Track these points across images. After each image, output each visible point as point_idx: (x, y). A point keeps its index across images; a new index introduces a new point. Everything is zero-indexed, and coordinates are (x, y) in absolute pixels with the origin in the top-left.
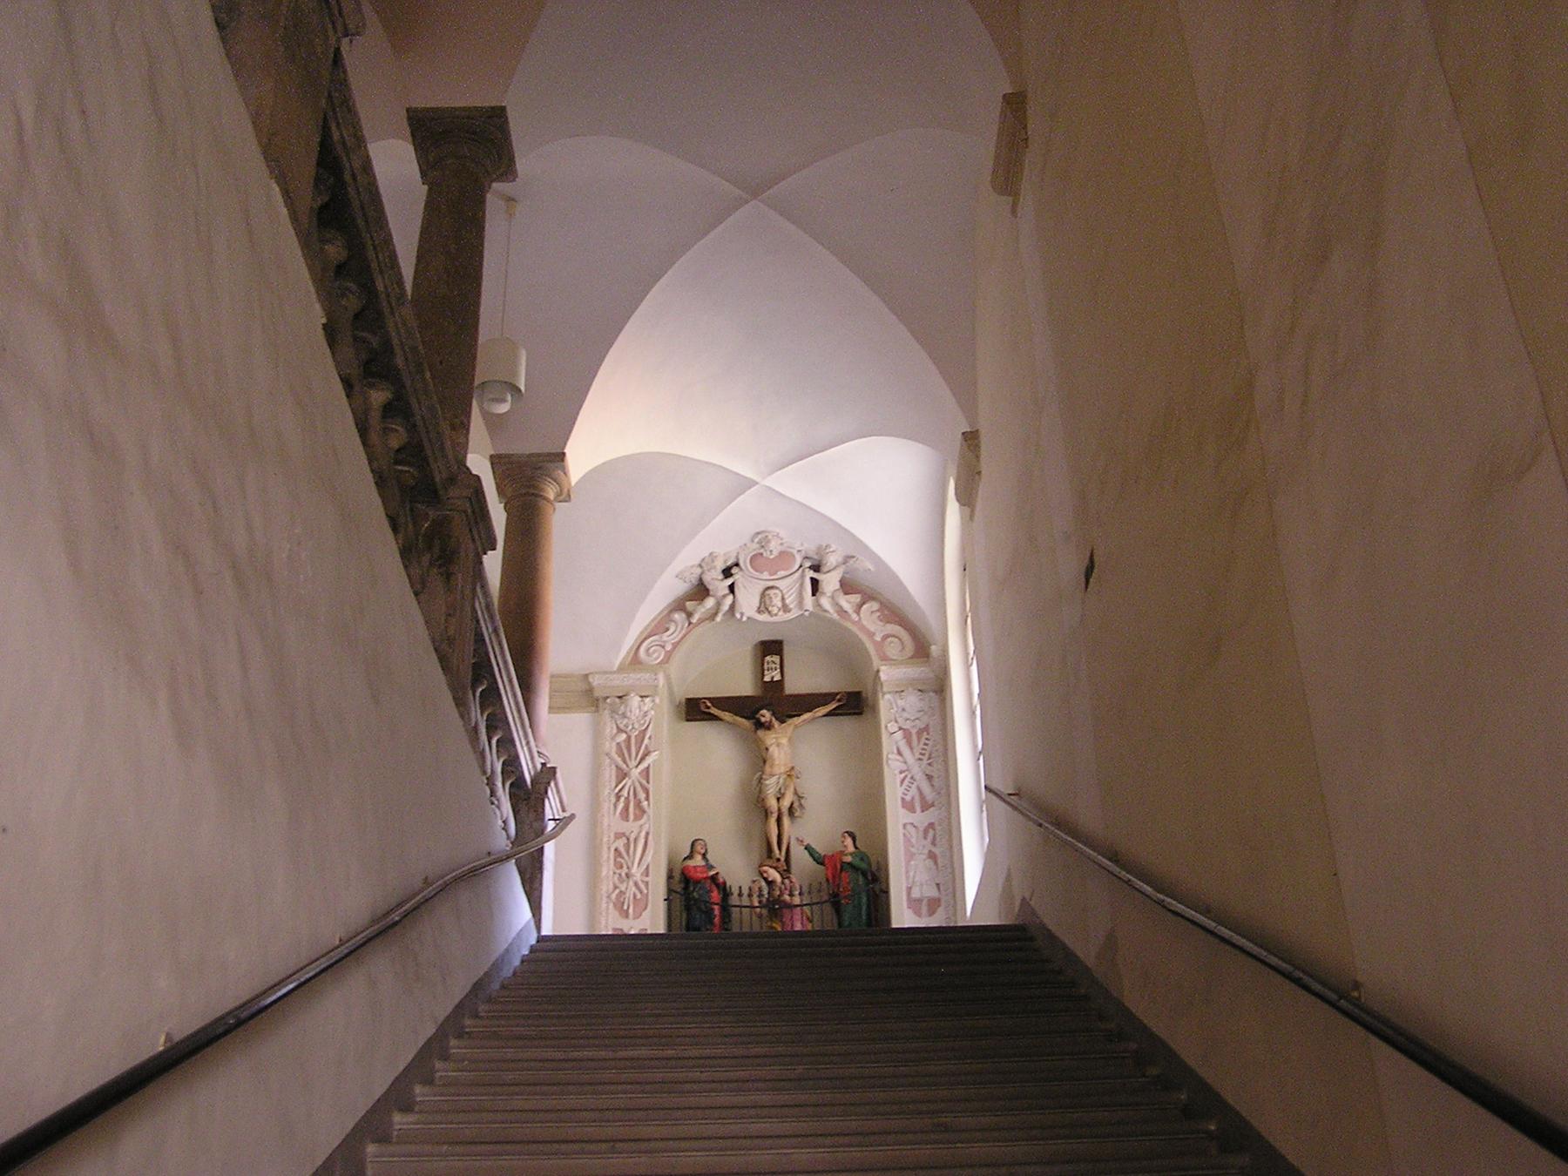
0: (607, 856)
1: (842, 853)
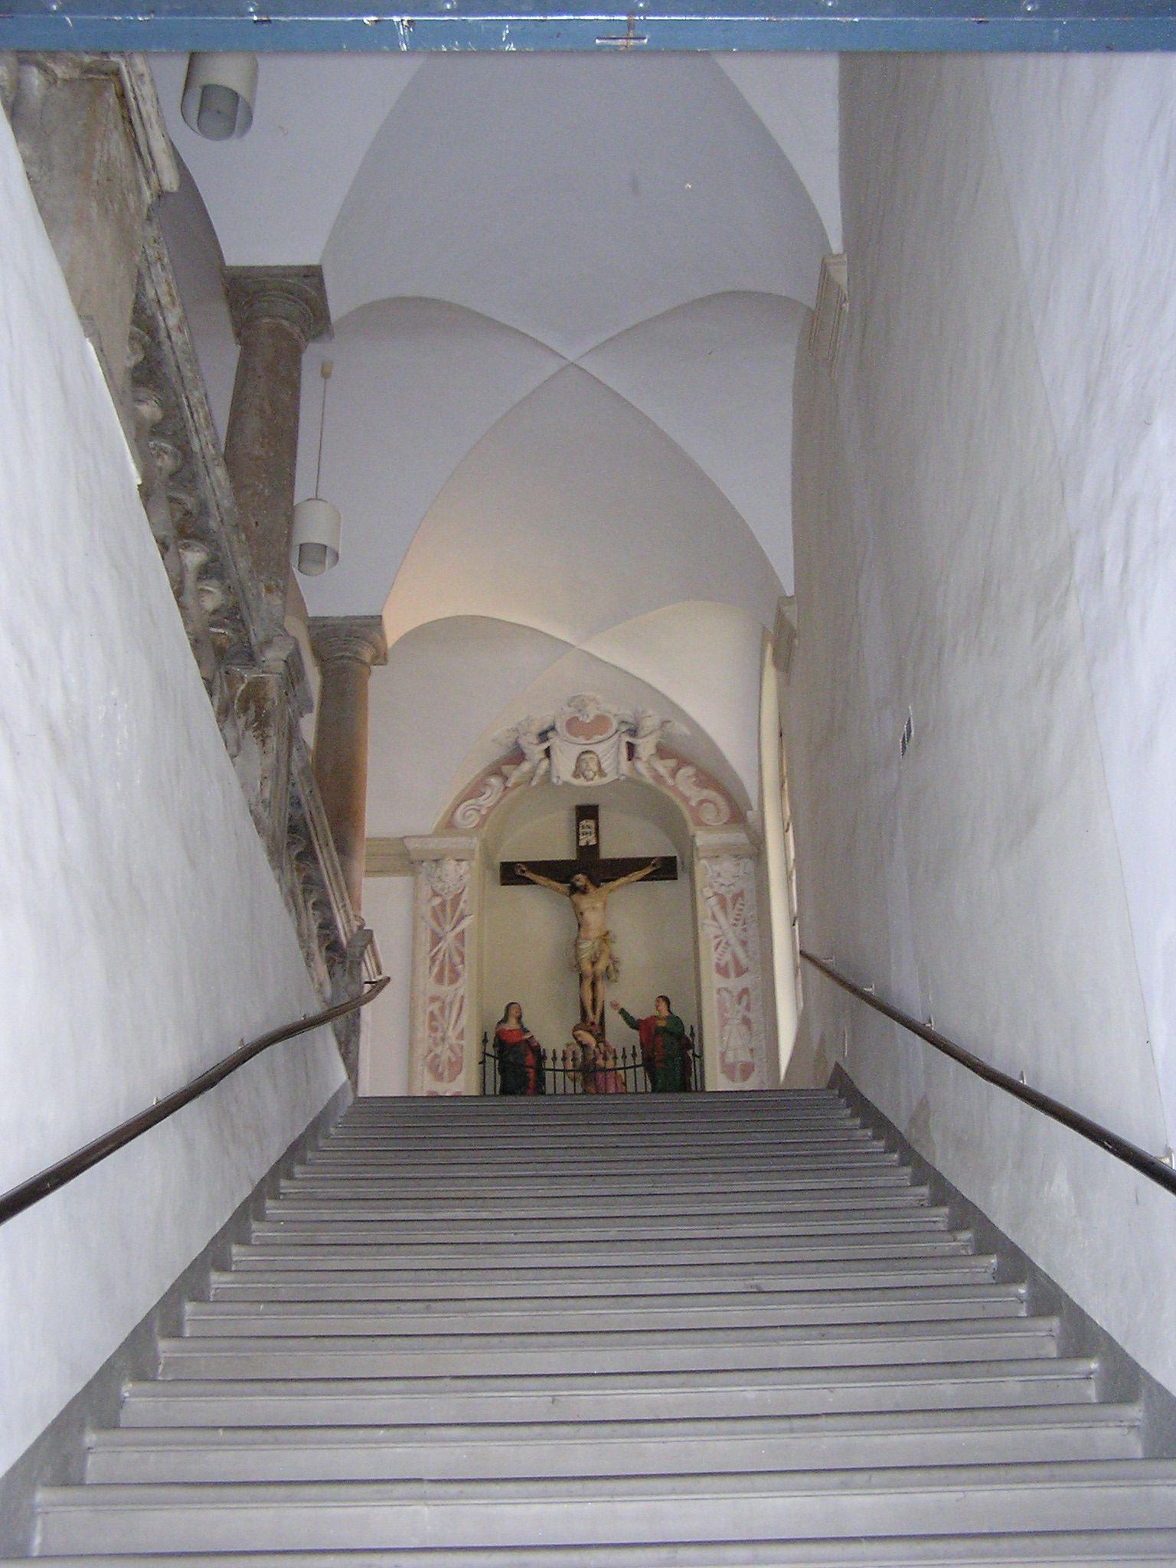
0: (422, 1019)
1: (654, 1018)
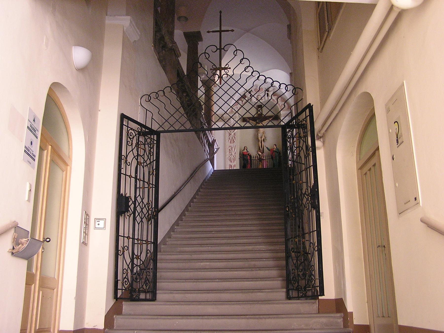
0: (228, 151)
1: (274, 149)
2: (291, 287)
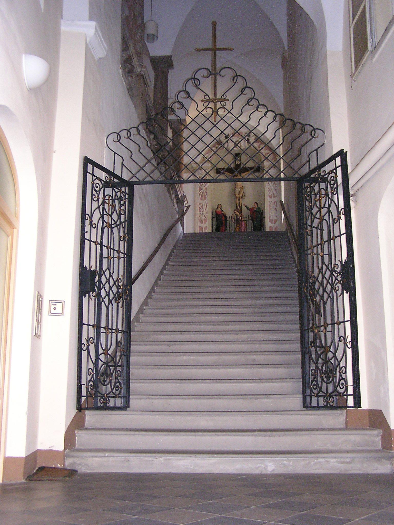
0: (197, 209)
1: (254, 208)
2: (308, 392)
